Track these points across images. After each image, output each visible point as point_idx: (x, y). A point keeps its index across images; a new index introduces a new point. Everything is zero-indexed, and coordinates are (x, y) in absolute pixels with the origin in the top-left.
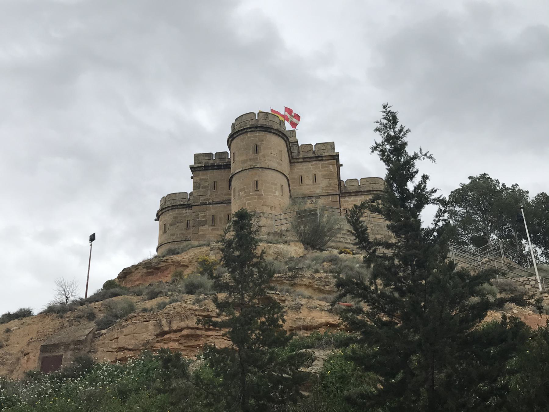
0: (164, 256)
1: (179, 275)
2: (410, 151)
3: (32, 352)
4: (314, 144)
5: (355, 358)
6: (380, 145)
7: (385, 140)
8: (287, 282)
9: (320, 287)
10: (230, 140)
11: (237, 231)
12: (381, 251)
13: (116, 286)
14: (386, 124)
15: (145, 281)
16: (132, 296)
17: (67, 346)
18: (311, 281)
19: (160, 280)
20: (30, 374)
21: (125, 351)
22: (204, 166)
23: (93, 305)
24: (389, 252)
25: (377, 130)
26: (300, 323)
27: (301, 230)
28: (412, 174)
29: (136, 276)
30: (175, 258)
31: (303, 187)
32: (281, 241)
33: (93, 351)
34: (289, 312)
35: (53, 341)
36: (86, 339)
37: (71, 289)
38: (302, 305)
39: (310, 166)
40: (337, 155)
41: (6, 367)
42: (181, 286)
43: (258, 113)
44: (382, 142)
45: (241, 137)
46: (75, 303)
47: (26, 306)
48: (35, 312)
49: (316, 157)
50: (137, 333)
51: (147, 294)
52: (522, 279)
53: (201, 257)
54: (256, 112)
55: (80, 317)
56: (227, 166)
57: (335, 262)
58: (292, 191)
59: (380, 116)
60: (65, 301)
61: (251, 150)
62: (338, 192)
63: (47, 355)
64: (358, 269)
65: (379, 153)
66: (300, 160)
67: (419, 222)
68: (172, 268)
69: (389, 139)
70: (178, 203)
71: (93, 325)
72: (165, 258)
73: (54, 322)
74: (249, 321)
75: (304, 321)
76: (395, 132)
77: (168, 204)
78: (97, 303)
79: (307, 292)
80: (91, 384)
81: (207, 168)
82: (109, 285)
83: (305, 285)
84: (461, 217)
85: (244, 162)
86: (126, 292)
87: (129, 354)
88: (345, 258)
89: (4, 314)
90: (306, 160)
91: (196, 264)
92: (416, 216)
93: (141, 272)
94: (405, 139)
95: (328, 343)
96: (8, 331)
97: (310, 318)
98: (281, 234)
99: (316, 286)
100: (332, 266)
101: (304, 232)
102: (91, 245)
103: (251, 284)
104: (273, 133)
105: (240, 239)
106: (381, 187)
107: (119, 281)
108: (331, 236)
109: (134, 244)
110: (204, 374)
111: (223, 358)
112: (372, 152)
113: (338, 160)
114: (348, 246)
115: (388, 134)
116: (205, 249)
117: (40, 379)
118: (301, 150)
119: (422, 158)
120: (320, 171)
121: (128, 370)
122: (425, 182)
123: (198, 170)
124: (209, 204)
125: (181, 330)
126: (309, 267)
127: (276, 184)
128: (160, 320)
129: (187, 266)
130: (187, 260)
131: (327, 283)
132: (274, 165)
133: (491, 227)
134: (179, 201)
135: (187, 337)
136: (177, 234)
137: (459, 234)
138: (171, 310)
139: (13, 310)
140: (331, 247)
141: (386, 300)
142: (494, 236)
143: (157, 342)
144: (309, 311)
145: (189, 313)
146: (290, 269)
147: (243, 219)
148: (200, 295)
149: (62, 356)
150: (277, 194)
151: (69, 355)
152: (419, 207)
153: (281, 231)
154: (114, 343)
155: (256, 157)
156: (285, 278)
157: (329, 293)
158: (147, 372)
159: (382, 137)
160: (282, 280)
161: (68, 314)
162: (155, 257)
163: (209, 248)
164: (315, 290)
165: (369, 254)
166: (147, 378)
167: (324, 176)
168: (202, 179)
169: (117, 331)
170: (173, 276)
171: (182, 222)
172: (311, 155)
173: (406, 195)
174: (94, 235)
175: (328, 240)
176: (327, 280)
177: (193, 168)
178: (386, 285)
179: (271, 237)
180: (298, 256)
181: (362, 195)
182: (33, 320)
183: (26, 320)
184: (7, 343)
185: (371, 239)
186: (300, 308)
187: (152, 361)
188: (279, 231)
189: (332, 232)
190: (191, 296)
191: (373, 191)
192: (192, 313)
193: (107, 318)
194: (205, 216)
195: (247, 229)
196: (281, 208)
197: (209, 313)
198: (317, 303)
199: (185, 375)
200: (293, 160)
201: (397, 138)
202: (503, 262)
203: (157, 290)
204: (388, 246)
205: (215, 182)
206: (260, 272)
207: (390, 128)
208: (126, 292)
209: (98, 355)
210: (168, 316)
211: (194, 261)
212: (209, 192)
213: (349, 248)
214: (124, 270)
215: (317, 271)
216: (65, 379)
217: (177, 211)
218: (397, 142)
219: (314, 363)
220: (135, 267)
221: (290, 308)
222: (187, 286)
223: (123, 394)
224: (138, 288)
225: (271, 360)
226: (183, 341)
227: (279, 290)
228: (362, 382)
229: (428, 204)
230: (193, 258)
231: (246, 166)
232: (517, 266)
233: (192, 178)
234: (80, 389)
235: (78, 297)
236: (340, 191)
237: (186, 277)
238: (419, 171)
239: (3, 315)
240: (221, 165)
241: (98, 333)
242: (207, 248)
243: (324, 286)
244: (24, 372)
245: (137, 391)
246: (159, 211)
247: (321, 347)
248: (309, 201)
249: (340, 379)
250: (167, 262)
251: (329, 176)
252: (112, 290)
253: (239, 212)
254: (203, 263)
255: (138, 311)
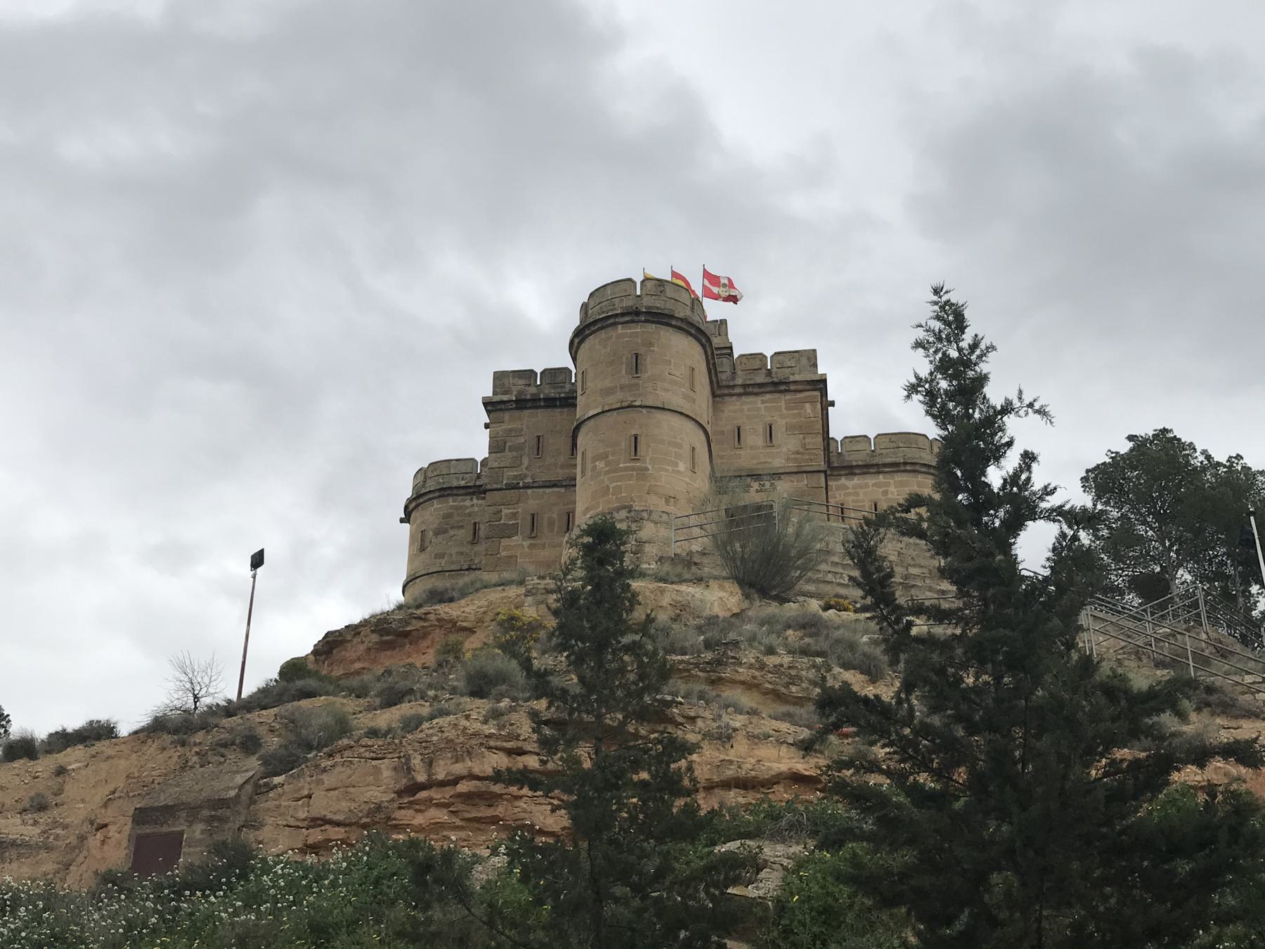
0: (419, 607)
1: (453, 650)
2: (995, 394)
3: (114, 823)
4: (769, 354)
5: (861, 880)
6: (926, 381)
7: (937, 369)
8: (701, 674)
9: (778, 687)
10: (576, 341)
11: (589, 568)
12: (920, 627)
13: (309, 674)
14: (940, 331)
15: (374, 661)
16: (344, 697)
17: (193, 811)
18: (757, 674)
19: (410, 660)
20: (108, 878)
21: (327, 827)
22: (515, 399)
23: (255, 717)
24: (943, 631)
25: (919, 345)
26: (730, 773)
27: (735, 552)
28: (998, 448)
29: (356, 649)
30: (444, 610)
31: (742, 452)
32: (687, 576)
33: (254, 824)
34: (705, 745)
35: (163, 800)
36: (238, 796)
37: (206, 680)
38: (735, 730)
39: (760, 405)
40: (823, 382)
41: (54, 855)
42: (456, 678)
43: (643, 282)
44: (931, 374)
45: (603, 334)
46: (214, 711)
47: (102, 716)
48: (124, 730)
49: (774, 384)
50: (352, 786)
51: (379, 694)
52: (1248, 679)
53: (503, 609)
54: (638, 279)
55: (225, 745)
56: (568, 402)
57: (813, 630)
58: (716, 461)
59: (926, 312)
60: (191, 705)
61: (624, 366)
62: (823, 466)
63: (148, 830)
64: (866, 649)
65: (921, 398)
66: (737, 390)
67: (1012, 562)
68: (438, 635)
69: (945, 366)
70: (455, 484)
71: (253, 764)
72: (422, 610)
73: (166, 754)
74: (614, 780)
75: (740, 767)
76: (960, 350)
77: (431, 485)
78: (264, 712)
79: (747, 700)
80: (247, 907)
81: (521, 404)
82: (292, 670)
83: (743, 683)
84: (1110, 528)
85: (609, 392)
86: (331, 688)
87: (336, 833)
88: (837, 620)
89: (52, 731)
90: (750, 390)
91: (493, 626)
92: (1006, 548)
93: (367, 640)
94: (983, 368)
95: (795, 827)
96: (61, 771)
97: (753, 761)
98: (689, 561)
99: (767, 685)
100: (807, 640)
101: (743, 558)
102: (254, 577)
103: (619, 693)
104: (675, 327)
105: (597, 587)
106: (923, 455)
107: (316, 661)
108: (805, 569)
109: (353, 575)
110: (507, 892)
111: (552, 863)
112: (908, 397)
113: (824, 391)
114: (843, 591)
115: (944, 354)
116: (513, 592)
117: (130, 891)
118: (738, 368)
119: (1022, 413)
120: (782, 417)
121: (332, 877)
122: (1029, 468)
123: (501, 410)
124: (524, 487)
125: (455, 781)
126: (752, 639)
127: (680, 446)
128: (408, 758)
129: (471, 631)
130: (472, 618)
131: (794, 680)
132: (677, 401)
133: (1177, 552)
134: (457, 479)
135: (468, 797)
136: (451, 555)
137: (1105, 567)
138: (432, 735)
139: (74, 723)
140: (804, 594)
141: (932, 741)
142: (1184, 575)
143: (400, 808)
144: (748, 744)
145: (473, 742)
146: (708, 645)
147: (604, 542)
148: (499, 701)
149: (182, 833)
150: (682, 467)
151: (198, 832)
152: (1015, 525)
153: (690, 553)
154: (302, 806)
155: (636, 381)
156: (697, 665)
157: (799, 701)
158: (377, 882)
159: (931, 362)
160: (688, 671)
161: (199, 737)
162: (400, 607)
163: (522, 590)
164: (766, 694)
165: (895, 632)
166: (375, 897)
167: (790, 428)
168: (511, 430)
169: (309, 779)
170: (439, 652)
171: (462, 527)
172: (760, 378)
173: (984, 499)
174: (262, 552)
175: (799, 578)
176: (793, 672)
177: (488, 404)
178: (934, 710)
179: (667, 567)
180: (728, 614)
181: (879, 473)
182: (117, 748)
183: (102, 746)
184: (59, 799)
185: (901, 599)
186: (729, 738)
187: (388, 856)
188: (684, 554)
189: (806, 558)
190: (478, 702)
191: (905, 464)
192: (482, 744)
193: (286, 747)
194: (514, 515)
195: (613, 565)
196: (689, 501)
197: (520, 744)
198: (769, 725)
199: (462, 894)
200: (720, 390)
201: (965, 362)
202: (1204, 636)
203: (402, 685)
204: (939, 615)
205: (539, 437)
206: (641, 665)
207: (949, 341)
208: (331, 688)
209: (266, 833)
210: (425, 748)
211: (487, 618)
212: (526, 461)
213: (846, 598)
214: (328, 634)
215: (771, 651)
216: (188, 893)
217: (451, 502)
218: (965, 372)
219: (762, 875)
220: (353, 629)
221: (707, 735)
222: (470, 679)
223: (320, 931)
224: (358, 678)
225: (661, 874)
226: (461, 807)
227: (682, 693)
228: (872, 924)
229: (1034, 520)
230: (485, 613)
231: (612, 401)
232: (1238, 648)
233: (487, 426)
234: (222, 918)
235: (221, 696)
236: (828, 462)
237: (468, 655)
238: (1016, 443)
239: (51, 735)
240: (555, 399)
241: (266, 784)
242: (521, 589)
243: (787, 685)
244: (96, 873)
245: (352, 924)
246: (410, 501)
247: (778, 836)
248: (756, 485)
249: (820, 913)
250: (425, 620)
251: (801, 429)
252: (300, 683)
253: (595, 524)
254: (511, 622)
255: (357, 733)
